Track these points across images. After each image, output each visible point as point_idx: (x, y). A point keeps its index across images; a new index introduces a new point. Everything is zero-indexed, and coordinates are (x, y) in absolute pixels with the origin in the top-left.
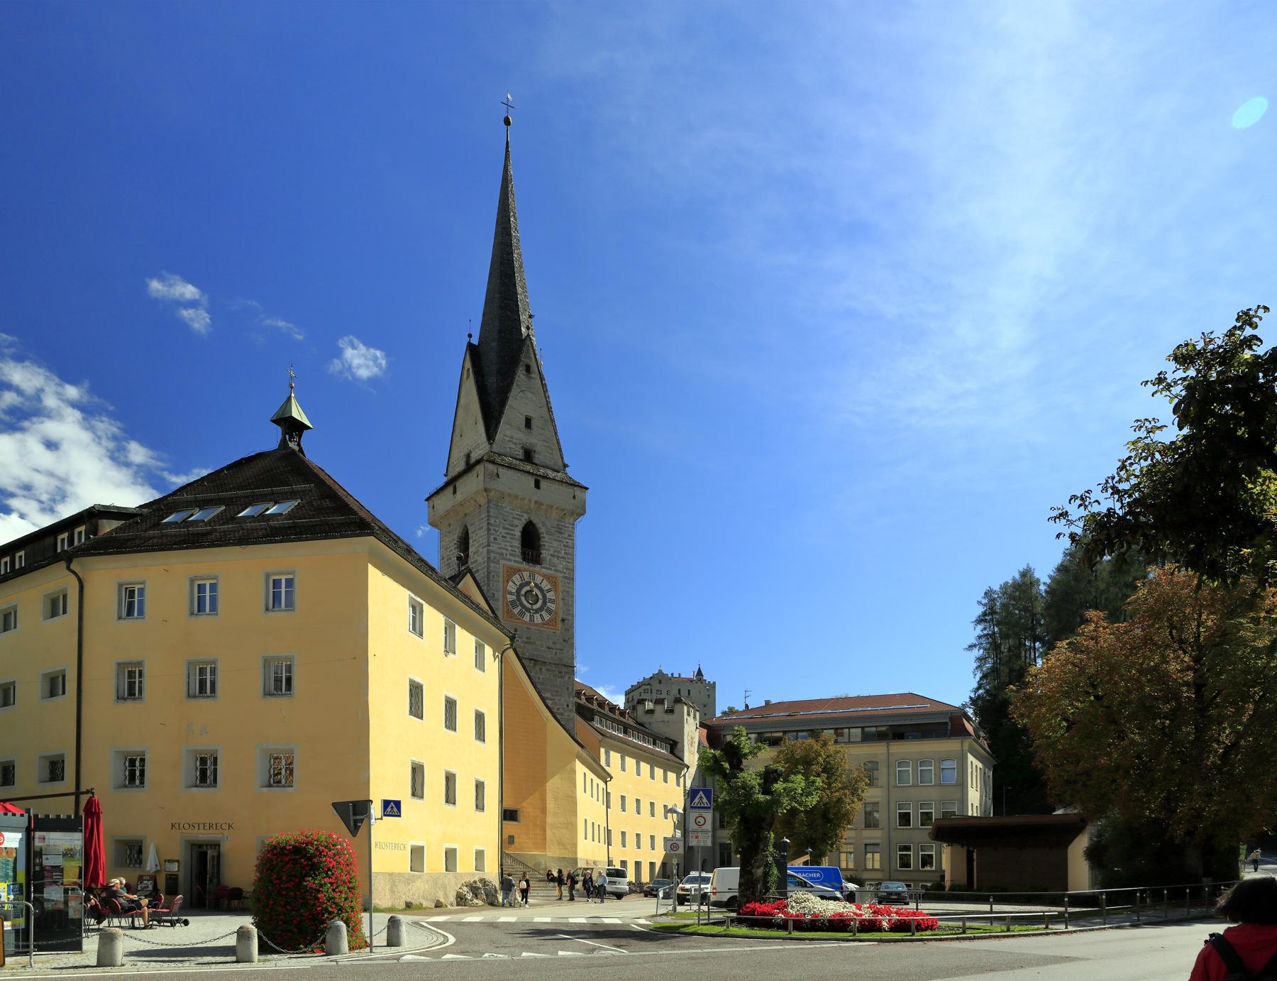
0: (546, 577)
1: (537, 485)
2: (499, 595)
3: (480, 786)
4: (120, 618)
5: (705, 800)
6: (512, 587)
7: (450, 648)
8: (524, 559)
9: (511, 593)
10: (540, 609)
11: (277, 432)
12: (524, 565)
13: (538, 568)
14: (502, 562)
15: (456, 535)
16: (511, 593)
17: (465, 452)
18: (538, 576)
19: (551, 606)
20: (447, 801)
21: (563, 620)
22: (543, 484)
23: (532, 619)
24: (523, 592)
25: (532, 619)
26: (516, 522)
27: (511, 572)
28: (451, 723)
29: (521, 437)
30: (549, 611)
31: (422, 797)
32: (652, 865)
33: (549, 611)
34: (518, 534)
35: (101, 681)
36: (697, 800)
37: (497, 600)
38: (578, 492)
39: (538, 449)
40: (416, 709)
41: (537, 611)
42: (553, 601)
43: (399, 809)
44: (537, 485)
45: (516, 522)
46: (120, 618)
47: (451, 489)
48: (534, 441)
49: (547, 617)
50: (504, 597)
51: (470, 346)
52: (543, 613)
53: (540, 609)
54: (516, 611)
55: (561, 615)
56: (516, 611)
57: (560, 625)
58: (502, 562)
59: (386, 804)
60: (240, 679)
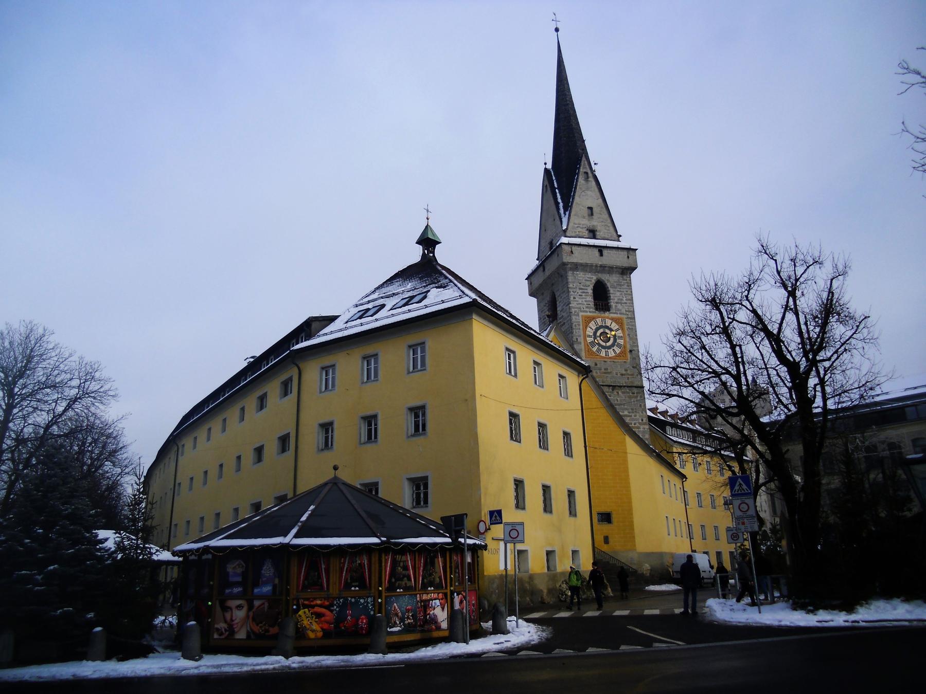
0: (612, 319)
1: (601, 255)
2: (581, 339)
3: (571, 494)
4: (321, 392)
5: (744, 487)
6: (590, 332)
7: (538, 381)
8: (596, 309)
9: (590, 336)
10: (613, 345)
11: (420, 248)
12: (597, 314)
13: (607, 314)
14: (581, 314)
15: (548, 298)
16: (590, 336)
17: (549, 241)
18: (607, 319)
19: (621, 342)
20: (545, 510)
21: (631, 351)
22: (605, 252)
23: (607, 353)
24: (598, 334)
25: (607, 353)
26: (588, 283)
27: (588, 320)
28: (543, 444)
29: (586, 222)
30: (619, 346)
31: (524, 508)
32: (731, 553)
33: (619, 346)
34: (590, 291)
35: (310, 437)
36: (737, 488)
37: (580, 343)
38: (631, 252)
39: (598, 228)
40: (515, 435)
41: (609, 348)
42: (621, 338)
43: (501, 517)
44: (601, 255)
45: (588, 283)
46: (321, 392)
47: (541, 268)
48: (595, 223)
49: (618, 350)
50: (585, 340)
51: (546, 169)
52: (615, 348)
53: (613, 345)
54: (595, 349)
55: (628, 348)
56: (595, 349)
57: (629, 355)
58: (581, 314)
59: (492, 513)
60: (392, 425)
